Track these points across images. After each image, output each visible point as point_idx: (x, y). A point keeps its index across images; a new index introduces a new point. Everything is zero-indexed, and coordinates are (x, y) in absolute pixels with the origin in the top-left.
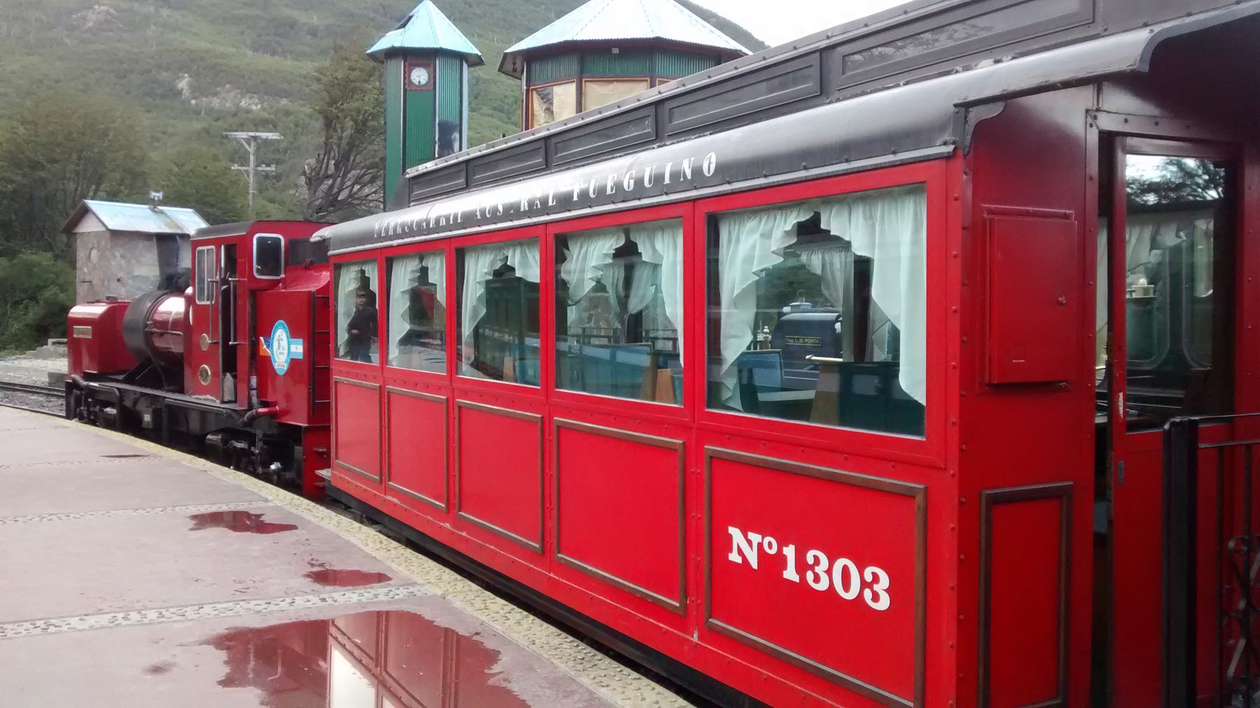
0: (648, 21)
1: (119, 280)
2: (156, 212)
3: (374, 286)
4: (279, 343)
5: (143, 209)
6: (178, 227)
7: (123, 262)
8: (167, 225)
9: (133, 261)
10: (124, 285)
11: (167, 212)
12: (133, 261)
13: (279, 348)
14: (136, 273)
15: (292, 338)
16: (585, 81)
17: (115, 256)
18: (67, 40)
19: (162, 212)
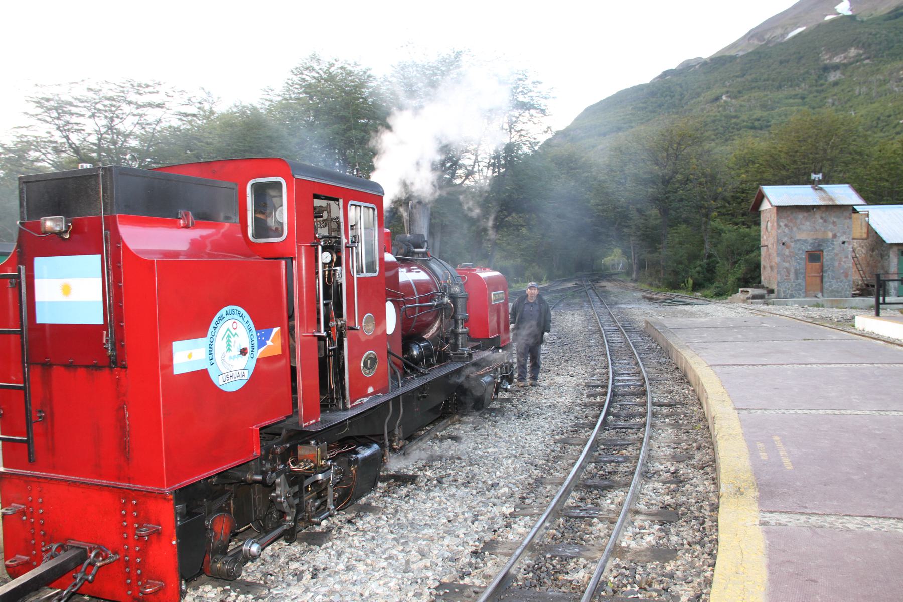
0: (83, 81)
1: (783, 244)
2: (816, 189)
3: (291, 339)
4: (229, 341)
5: (808, 188)
6: (831, 199)
7: (786, 230)
8: (822, 199)
9: (795, 229)
10: (788, 247)
11: (825, 189)
12: (795, 229)
13: (229, 350)
14: (798, 237)
15: (205, 372)
16: (352, 205)
17: (780, 226)
18: (897, 89)
19: (821, 189)
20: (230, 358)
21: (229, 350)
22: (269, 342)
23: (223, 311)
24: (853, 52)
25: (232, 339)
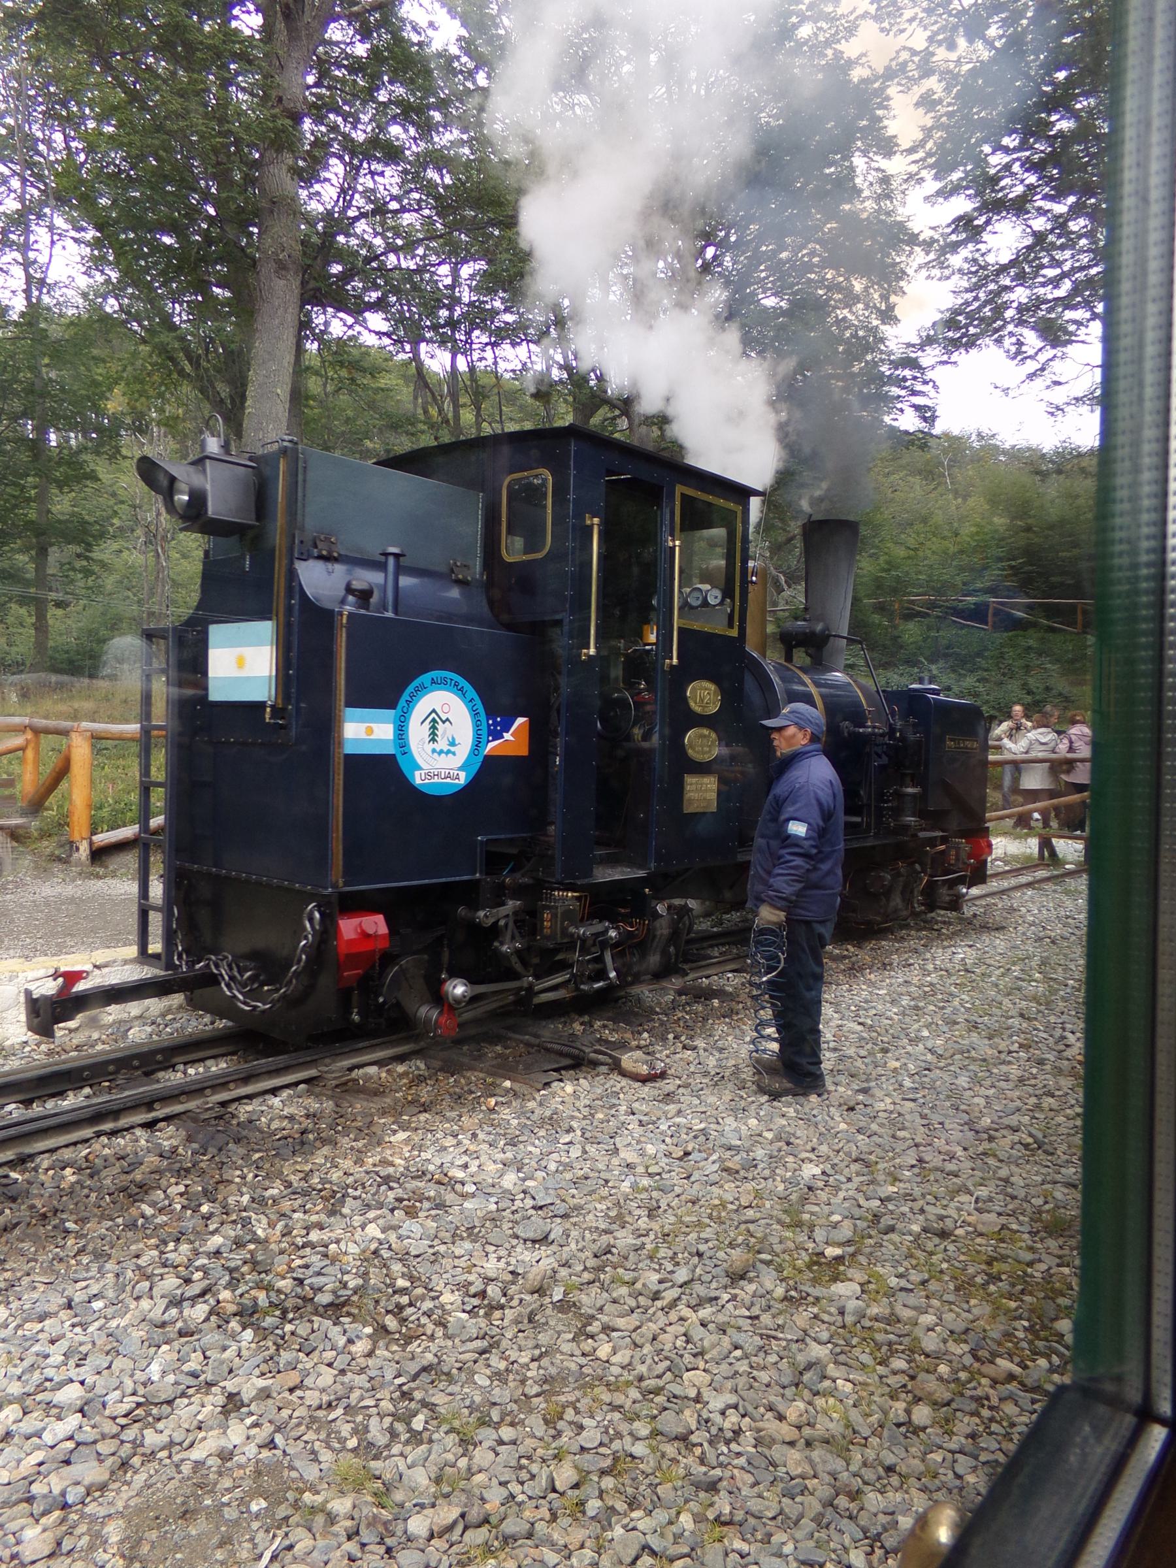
15: (392, 757)
20: (434, 751)
21: (433, 740)
22: (507, 736)
23: (426, 678)
24: (672, 949)
25: (440, 726)
